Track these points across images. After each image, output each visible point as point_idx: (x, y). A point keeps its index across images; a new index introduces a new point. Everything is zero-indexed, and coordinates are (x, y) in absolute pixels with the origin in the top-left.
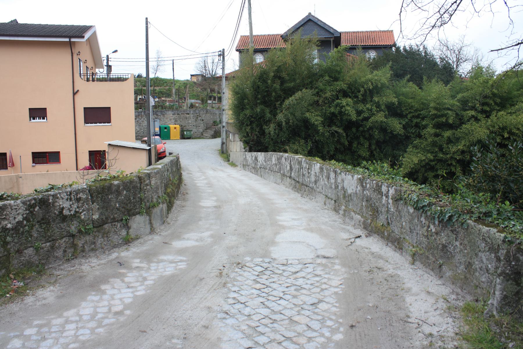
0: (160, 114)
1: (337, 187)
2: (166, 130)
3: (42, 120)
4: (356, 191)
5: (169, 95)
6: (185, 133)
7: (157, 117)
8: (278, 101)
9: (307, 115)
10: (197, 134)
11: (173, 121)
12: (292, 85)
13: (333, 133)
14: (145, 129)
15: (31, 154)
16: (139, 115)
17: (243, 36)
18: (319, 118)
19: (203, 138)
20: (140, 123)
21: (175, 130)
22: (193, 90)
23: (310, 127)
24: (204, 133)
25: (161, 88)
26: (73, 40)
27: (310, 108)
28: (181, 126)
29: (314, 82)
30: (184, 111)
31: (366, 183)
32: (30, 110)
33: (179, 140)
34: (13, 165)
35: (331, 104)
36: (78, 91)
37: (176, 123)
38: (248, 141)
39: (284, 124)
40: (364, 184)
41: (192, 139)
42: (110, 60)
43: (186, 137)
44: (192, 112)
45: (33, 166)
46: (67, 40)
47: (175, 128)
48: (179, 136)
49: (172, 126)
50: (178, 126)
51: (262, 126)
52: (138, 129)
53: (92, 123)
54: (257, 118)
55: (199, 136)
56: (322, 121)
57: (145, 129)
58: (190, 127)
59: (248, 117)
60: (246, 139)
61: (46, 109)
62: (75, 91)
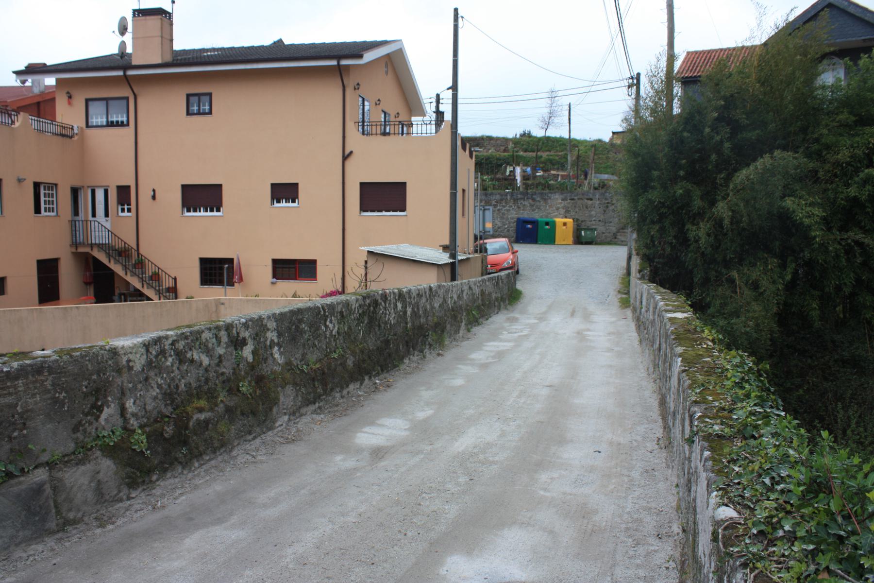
0: (538, 199)
2: (547, 227)
5: (562, 167)
7: (533, 203)
8: (720, 172)
9: (789, 202)
10: (605, 236)
11: (562, 211)
12: (753, 135)
13: (849, 245)
14: (512, 225)
16: (502, 200)
17: (692, 53)
18: (818, 212)
19: (616, 244)
20: (503, 214)
21: (565, 227)
22: (608, 158)
23: (794, 231)
24: (619, 234)
25: (552, 153)
26: (344, 62)
27: (797, 186)
29: (811, 129)
30: (583, 194)
32: (273, 186)
34: (241, 279)
35: (851, 178)
36: (351, 152)
38: (651, 256)
39: (726, 222)
41: (597, 244)
42: (441, 101)
43: (584, 241)
44: (597, 196)
45: (273, 283)
46: (334, 63)
47: (565, 224)
48: (570, 239)
49: (559, 221)
50: (569, 221)
51: (684, 225)
52: (499, 224)
53: (389, 211)
54: (675, 208)
55: (609, 239)
56: (824, 219)
57: (512, 225)
58: (594, 222)
59: (656, 206)
60: (647, 252)
61: (297, 184)
62: (347, 152)
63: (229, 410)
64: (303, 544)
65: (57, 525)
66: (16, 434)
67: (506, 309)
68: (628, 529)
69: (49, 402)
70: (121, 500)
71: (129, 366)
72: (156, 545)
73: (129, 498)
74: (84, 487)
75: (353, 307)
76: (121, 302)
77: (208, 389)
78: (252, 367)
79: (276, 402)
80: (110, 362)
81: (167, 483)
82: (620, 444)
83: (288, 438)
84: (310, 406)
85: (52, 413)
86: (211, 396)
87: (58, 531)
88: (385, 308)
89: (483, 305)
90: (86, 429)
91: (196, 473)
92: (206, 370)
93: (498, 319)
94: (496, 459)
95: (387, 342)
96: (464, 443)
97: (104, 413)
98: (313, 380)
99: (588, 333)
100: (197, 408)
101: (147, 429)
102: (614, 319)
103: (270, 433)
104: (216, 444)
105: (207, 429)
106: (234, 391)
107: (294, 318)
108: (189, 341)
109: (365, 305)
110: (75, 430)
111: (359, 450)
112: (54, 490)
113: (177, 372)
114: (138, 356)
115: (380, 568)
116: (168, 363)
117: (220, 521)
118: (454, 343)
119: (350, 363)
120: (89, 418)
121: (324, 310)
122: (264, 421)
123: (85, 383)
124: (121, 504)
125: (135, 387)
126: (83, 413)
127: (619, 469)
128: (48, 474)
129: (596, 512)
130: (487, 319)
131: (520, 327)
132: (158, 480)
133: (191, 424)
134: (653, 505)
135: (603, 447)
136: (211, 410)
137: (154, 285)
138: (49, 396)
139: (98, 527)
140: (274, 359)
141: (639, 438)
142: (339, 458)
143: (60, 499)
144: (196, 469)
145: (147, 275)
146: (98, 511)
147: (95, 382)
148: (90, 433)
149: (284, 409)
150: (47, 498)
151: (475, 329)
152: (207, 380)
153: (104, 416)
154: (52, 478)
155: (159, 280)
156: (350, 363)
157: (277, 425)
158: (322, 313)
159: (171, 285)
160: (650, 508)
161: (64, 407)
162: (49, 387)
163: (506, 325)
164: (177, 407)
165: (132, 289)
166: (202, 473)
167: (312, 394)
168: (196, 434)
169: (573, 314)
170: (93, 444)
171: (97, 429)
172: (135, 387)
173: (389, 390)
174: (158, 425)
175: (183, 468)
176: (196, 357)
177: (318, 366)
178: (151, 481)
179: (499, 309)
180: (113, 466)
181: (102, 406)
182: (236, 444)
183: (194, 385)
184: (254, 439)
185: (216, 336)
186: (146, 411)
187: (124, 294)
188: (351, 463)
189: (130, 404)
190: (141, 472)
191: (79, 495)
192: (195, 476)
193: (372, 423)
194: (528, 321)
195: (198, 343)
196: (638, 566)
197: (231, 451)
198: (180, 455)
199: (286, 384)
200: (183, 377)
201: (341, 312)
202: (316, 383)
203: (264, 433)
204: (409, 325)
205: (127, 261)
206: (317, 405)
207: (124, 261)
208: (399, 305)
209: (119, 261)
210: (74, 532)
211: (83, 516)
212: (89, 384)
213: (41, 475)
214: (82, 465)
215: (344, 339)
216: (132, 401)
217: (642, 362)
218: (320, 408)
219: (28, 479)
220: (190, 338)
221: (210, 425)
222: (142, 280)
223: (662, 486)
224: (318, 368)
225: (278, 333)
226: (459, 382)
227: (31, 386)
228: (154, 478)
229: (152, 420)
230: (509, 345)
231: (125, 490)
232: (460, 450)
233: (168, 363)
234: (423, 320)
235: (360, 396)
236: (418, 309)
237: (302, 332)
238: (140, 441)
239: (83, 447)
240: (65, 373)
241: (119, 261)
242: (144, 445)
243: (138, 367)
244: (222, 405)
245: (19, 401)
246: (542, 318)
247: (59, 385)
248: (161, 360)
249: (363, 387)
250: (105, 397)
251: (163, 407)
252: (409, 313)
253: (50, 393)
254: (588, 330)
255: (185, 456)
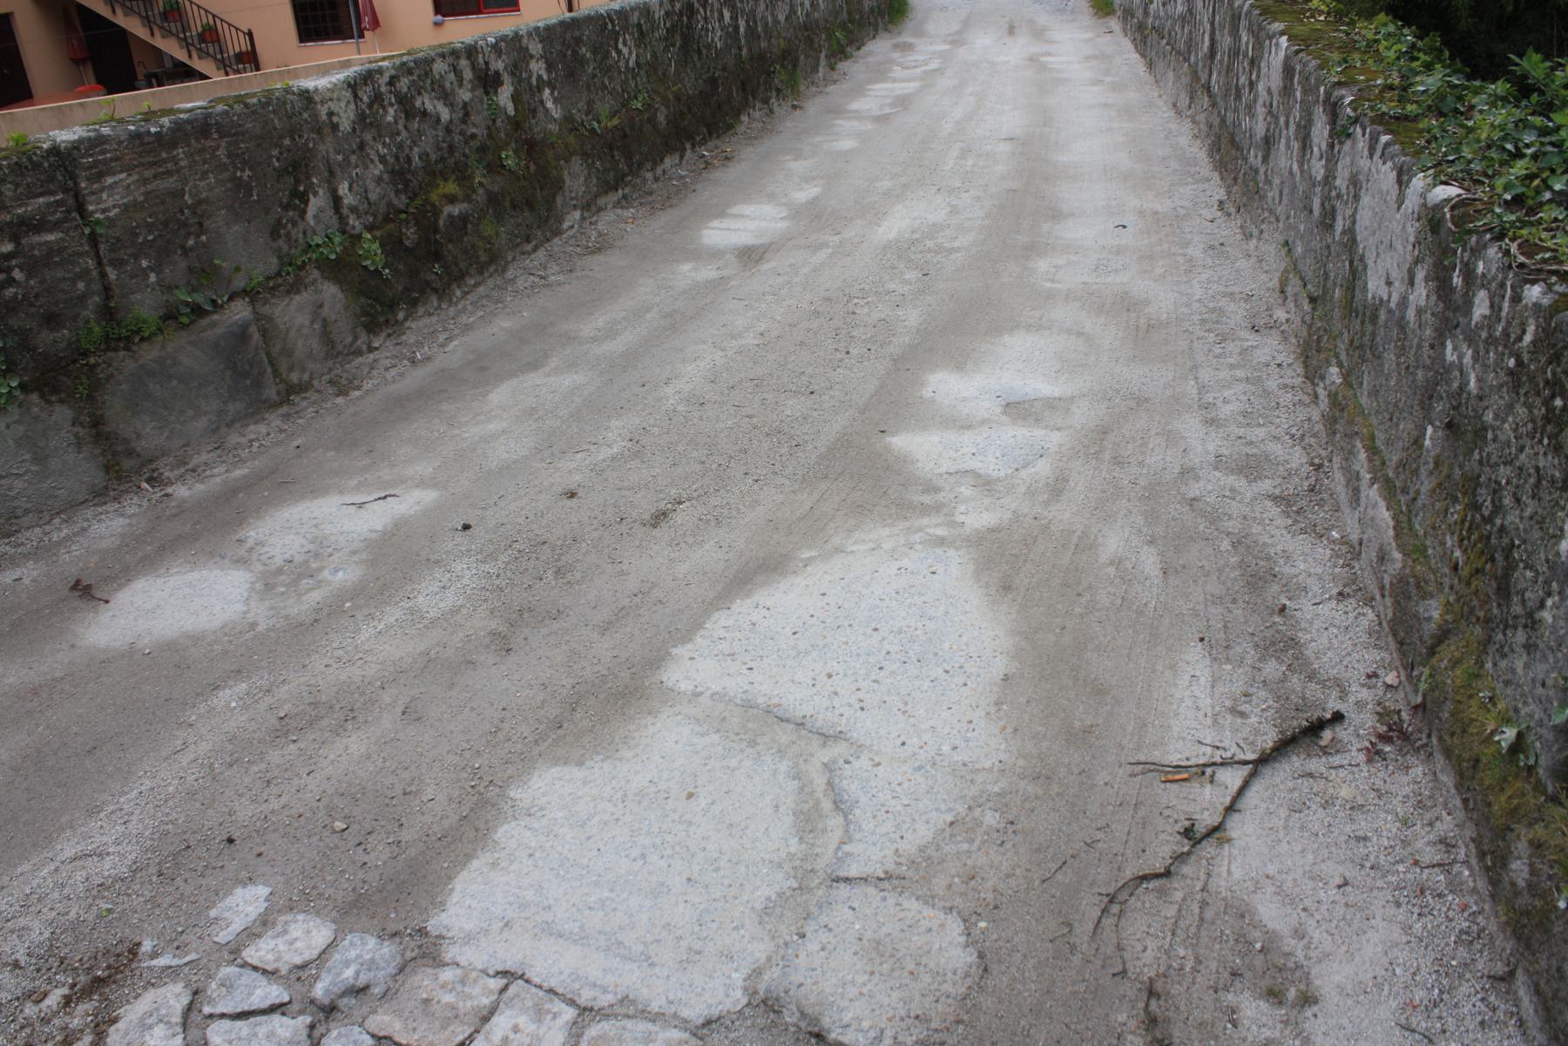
1: (1329, 216)
4: (1403, 303)
31: (1468, 274)
34: (375, 23)
40: (1457, 280)
63: (493, 199)
64: (686, 379)
65: (278, 393)
66: (191, 242)
67: (886, 30)
68: (1203, 321)
69: (229, 185)
70: (359, 353)
71: (332, 122)
72: (444, 408)
73: (371, 350)
74: (305, 331)
75: (656, 16)
76: (152, 87)
77: (456, 163)
78: (516, 124)
79: (559, 185)
80: (305, 115)
81: (421, 323)
82: (1157, 213)
83: (588, 247)
84: (610, 194)
85: (237, 205)
86: (463, 176)
87: (281, 404)
88: (706, 19)
89: (850, 21)
90: (289, 233)
91: (460, 307)
92: (448, 130)
93: (879, 48)
94: (956, 244)
95: (713, 81)
96: (896, 224)
97: (310, 204)
98: (611, 148)
99: (1050, 59)
100: (445, 196)
101: (378, 233)
102: (1088, 35)
103: (556, 240)
104: (483, 258)
105: (466, 233)
106: (495, 167)
107: (568, 36)
108: (415, 78)
109: (674, 12)
110: (274, 234)
111: (715, 254)
112: (264, 336)
113: (404, 133)
114: (343, 105)
115: (827, 397)
116: (390, 119)
117: (533, 366)
118: (814, 89)
119: (661, 118)
120: (291, 213)
121: (612, 21)
122: (547, 220)
123: (275, 152)
124: (360, 360)
125: (346, 159)
126: (281, 205)
127: (1166, 246)
128: (250, 309)
129: (1147, 302)
130: (859, 48)
131: (921, 58)
132: (406, 319)
133: (441, 223)
134: (1236, 289)
135: (1129, 219)
136: (468, 199)
137: (211, 50)
138: (226, 175)
139: (338, 395)
140: (547, 110)
141: (1186, 204)
142: (686, 267)
143: (276, 350)
144: (459, 300)
145: (194, 33)
146: (331, 370)
147: (289, 151)
148: (296, 241)
149: (572, 199)
150: (257, 349)
151: (842, 66)
152: (451, 148)
153: (311, 211)
154: (258, 317)
155: (218, 40)
156: (661, 118)
157: (565, 226)
158: (610, 27)
159: (244, 49)
160: (1232, 294)
161: (252, 195)
162: (225, 160)
163: (896, 55)
164: (416, 195)
165: (169, 64)
166: (469, 307)
167: (612, 173)
168: (450, 241)
169: (1011, 30)
170: (304, 258)
171: (304, 233)
172: (346, 159)
173: (730, 164)
174: (391, 226)
175: (440, 299)
176: (429, 107)
177: (615, 122)
178: (397, 321)
179: (876, 30)
180: (340, 295)
181: (305, 193)
182: (510, 258)
183: (433, 157)
184: (534, 250)
185: (455, 69)
186: (369, 203)
187: (155, 75)
188: (709, 273)
189: (343, 189)
190: (381, 304)
191: (300, 343)
192: (459, 311)
193: (722, 214)
194: (931, 48)
195: (429, 81)
196: (1232, 367)
197: (504, 270)
198: (433, 277)
199: (572, 154)
200: (415, 143)
201: (639, 26)
202: (616, 153)
203: (548, 240)
204: (744, 52)
205: (149, 8)
206: (620, 191)
207: (142, 10)
208: (727, 15)
209: (132, 9)
210: (304, 404)
211: (311, 378)
212: (281, 153)
213: (240, 311)
214: (296, 293)
215: (648, 76)
216: (346, 185)
217: (1160, 96)
218: (625, 197)
219: (225, 317)
220: (417, 72)
221: (469, 226)
222: (186, 44)
223: (1242, 264)
224: (615, 127)
225: (546, 62)
226: (847, 144)
227: (197, 158)
228: (401, 316)
229: (380, 218)
230: (913, 86)
231: (363, 337)
232: (892, 236)
233: (390, 119)
234: (763, 44)
235: (682, 177)
236: (755, 22)
237: (583, 62)
238: (372, 251)
239: (290, 264)
240: (243, 134)
241: (132, 9)
242: (380, 259)
243: (345, 125)
244: (481, 191)
245: (186, 185)
246: (957, 40)
247: (237, 155)
248: (377, 112)
249: (684, 162)
250: (308, 178)
251: (392, 195)
252: (742, 29)
253: (228, 170)
254: (1049, 54)
255: (441, 277)
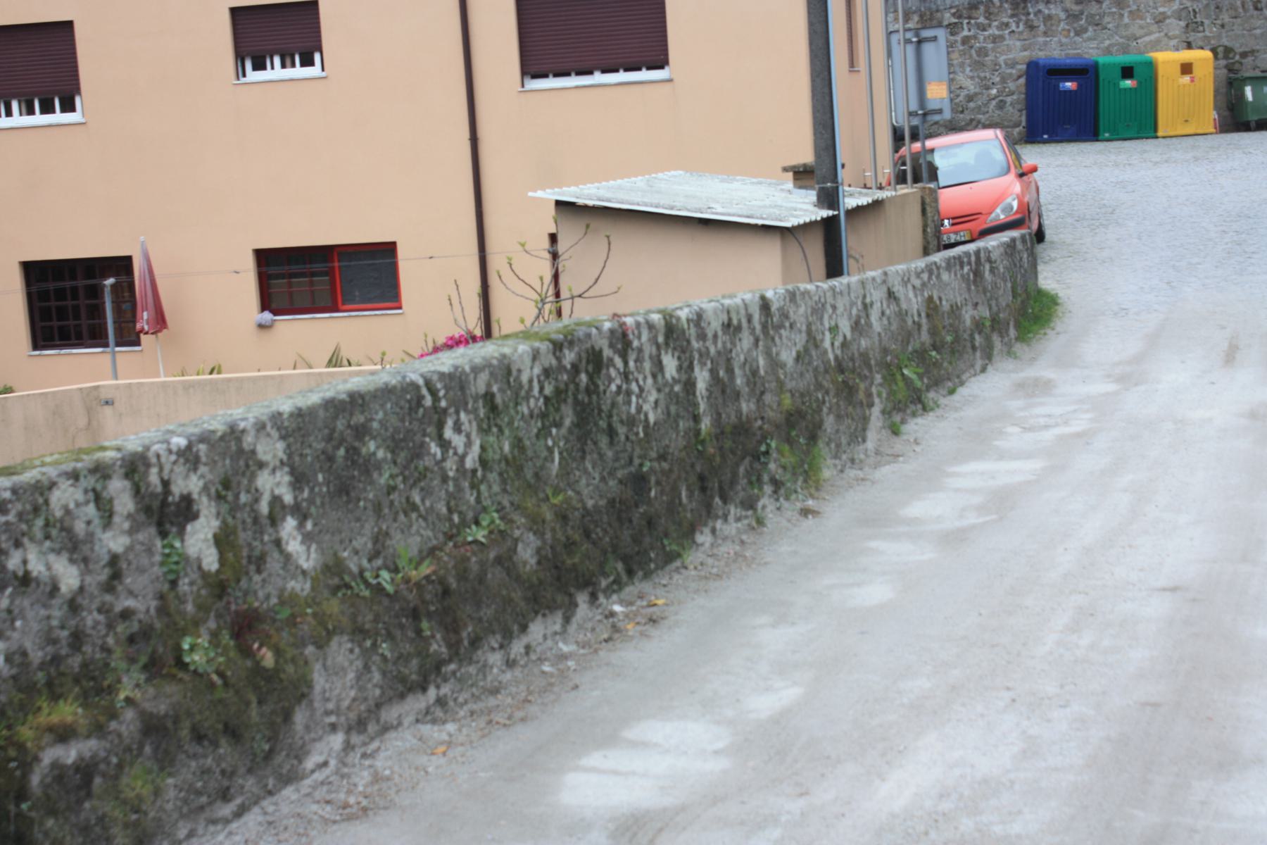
2: (1128, 83)
3: (299, 72)
6: (1248, 92)
15: (249, 264)
20: (982, 52)
21: (1187, 79)
28: (1222, 53)
33: (1213, 136)
34: (160, 321)
37: (1192, 37)
43: (1253, 117)
47: (1186, 69)
48: (1209, 115)
49: (1167, 59)
52: (971, 86)
53: (566, 74)
57: (1011, 85)
